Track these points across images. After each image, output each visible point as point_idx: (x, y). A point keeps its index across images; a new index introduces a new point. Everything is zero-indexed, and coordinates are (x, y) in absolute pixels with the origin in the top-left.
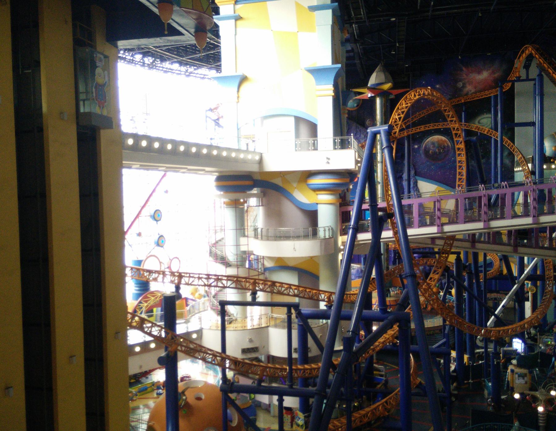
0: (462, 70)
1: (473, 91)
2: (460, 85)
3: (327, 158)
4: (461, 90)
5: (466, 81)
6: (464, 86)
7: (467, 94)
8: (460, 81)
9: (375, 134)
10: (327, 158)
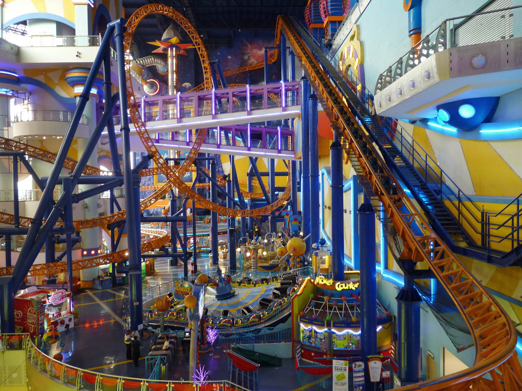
0: (247, 46)
1: (256, 62)
2: (246, 57)
3: (78, 52)
4: (246, 61)
5: (251, 55)
6: (249, 59)
7: (251, 65)
8: (246, 54)
9: (113, 28)
10: (78, 52)
